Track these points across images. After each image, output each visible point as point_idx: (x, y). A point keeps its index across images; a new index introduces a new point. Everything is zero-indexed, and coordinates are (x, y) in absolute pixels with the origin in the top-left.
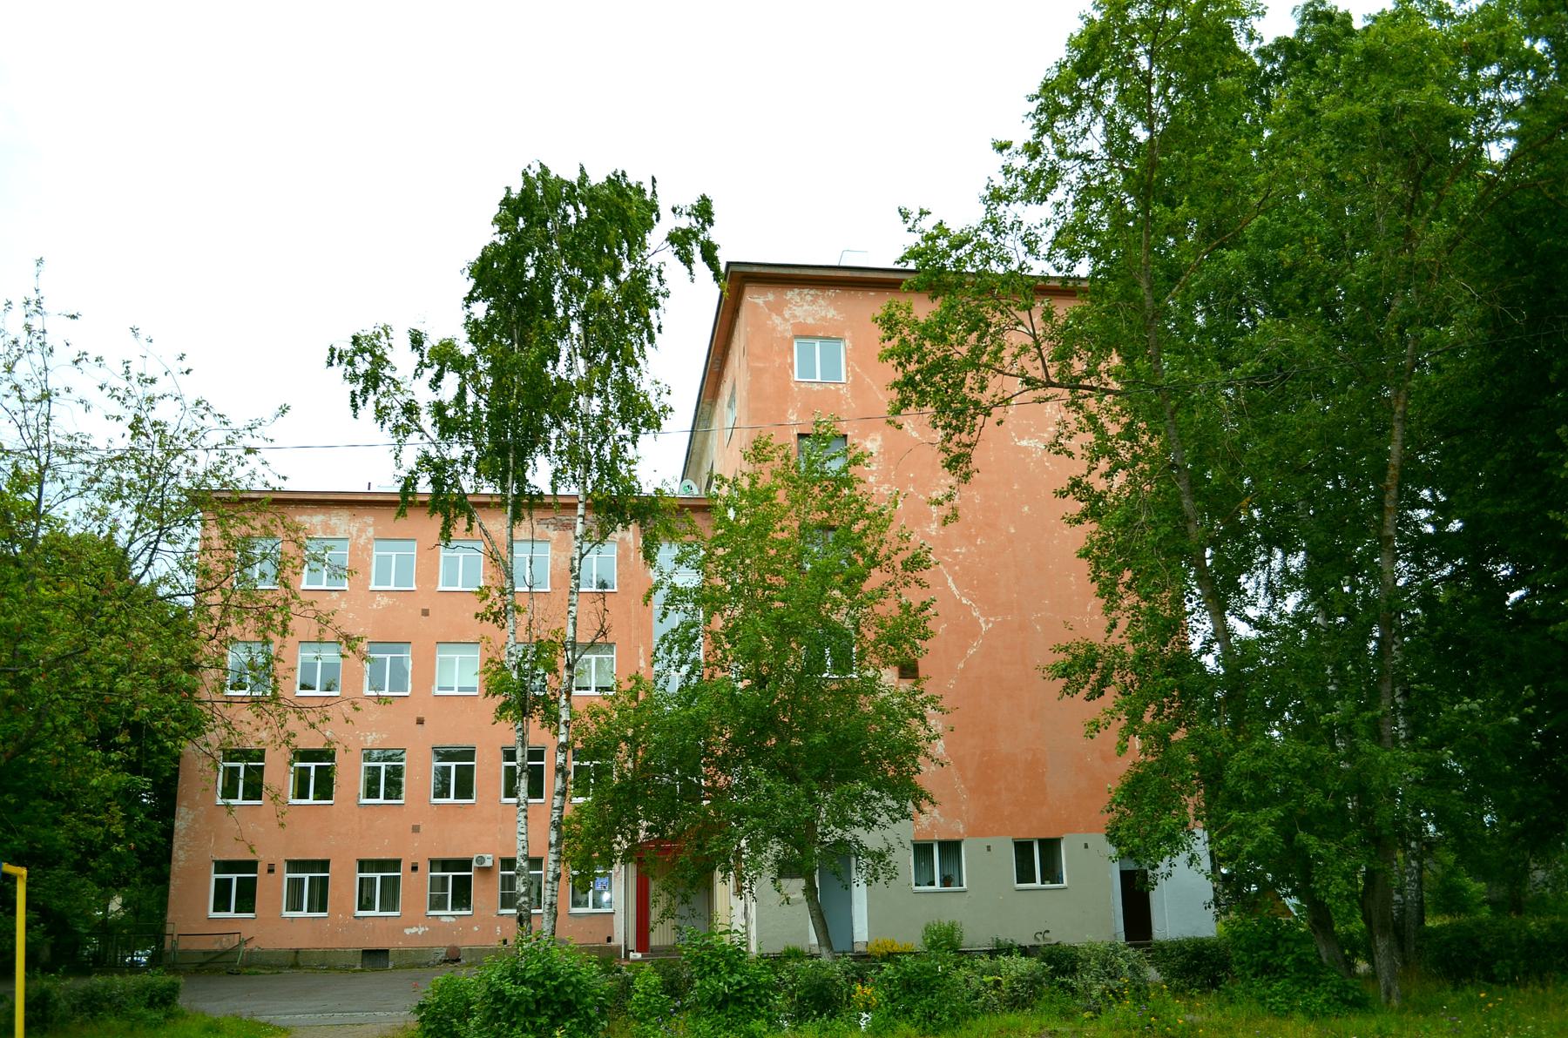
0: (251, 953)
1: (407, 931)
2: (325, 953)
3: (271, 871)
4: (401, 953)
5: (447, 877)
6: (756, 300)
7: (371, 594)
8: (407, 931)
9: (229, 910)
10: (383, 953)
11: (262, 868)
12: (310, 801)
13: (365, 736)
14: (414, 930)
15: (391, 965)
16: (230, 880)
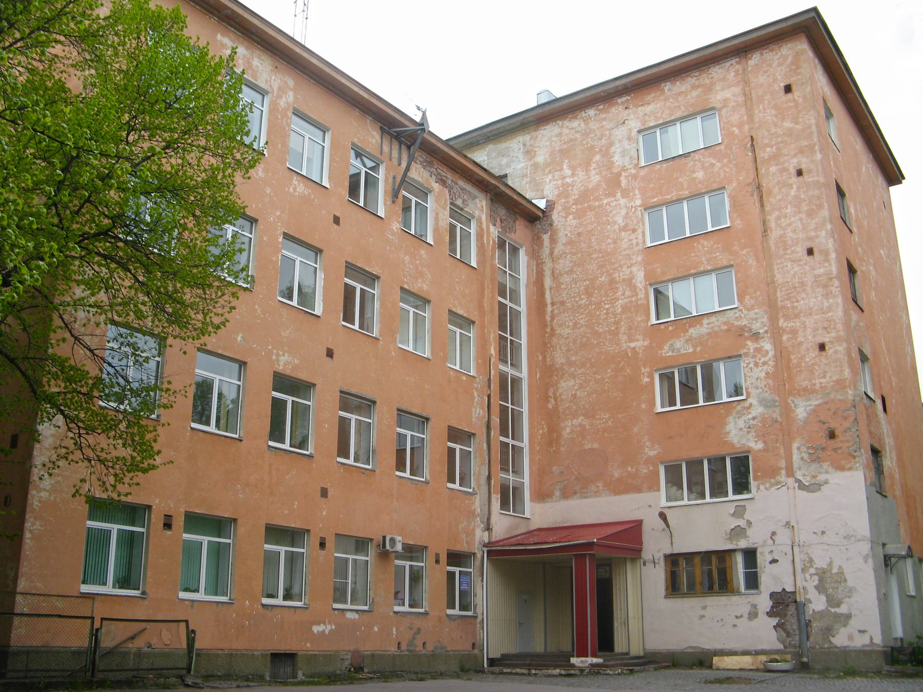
0: (139, 654)
1: (316, 629)
2: (231, 656)
3: (168, 526)
4: (312, 658)
5: (347, 560)
6: (802, 46)
7: (288, 173)
8: (316, 629)
9: (105, 584)
10: (290, 657)
11: (157, 520)
12: (678, 407)
13: (278, 355)
14: (321, 628)
15: (300, 676)
16: (109, 532)
